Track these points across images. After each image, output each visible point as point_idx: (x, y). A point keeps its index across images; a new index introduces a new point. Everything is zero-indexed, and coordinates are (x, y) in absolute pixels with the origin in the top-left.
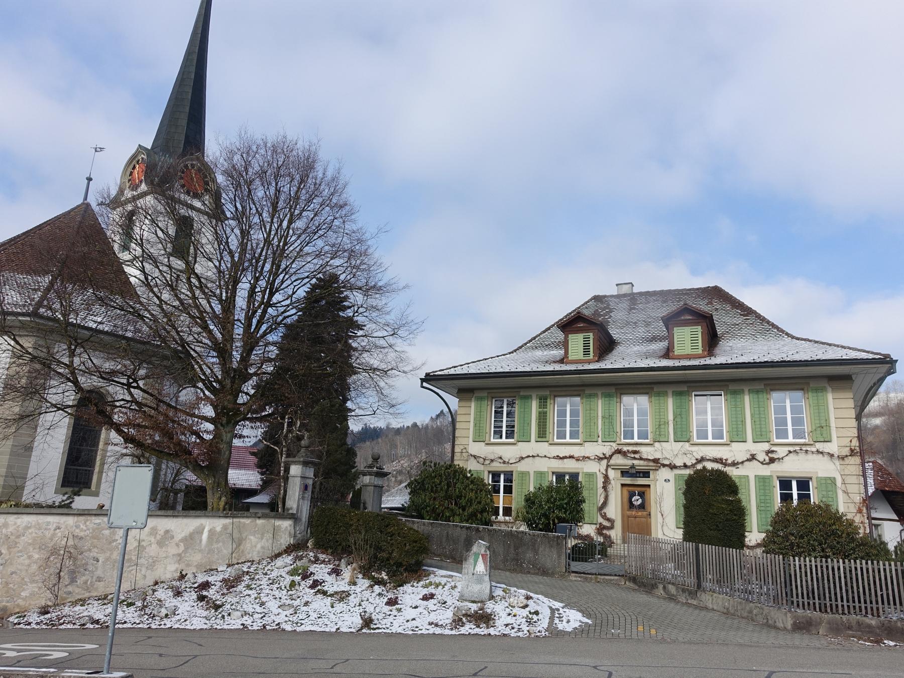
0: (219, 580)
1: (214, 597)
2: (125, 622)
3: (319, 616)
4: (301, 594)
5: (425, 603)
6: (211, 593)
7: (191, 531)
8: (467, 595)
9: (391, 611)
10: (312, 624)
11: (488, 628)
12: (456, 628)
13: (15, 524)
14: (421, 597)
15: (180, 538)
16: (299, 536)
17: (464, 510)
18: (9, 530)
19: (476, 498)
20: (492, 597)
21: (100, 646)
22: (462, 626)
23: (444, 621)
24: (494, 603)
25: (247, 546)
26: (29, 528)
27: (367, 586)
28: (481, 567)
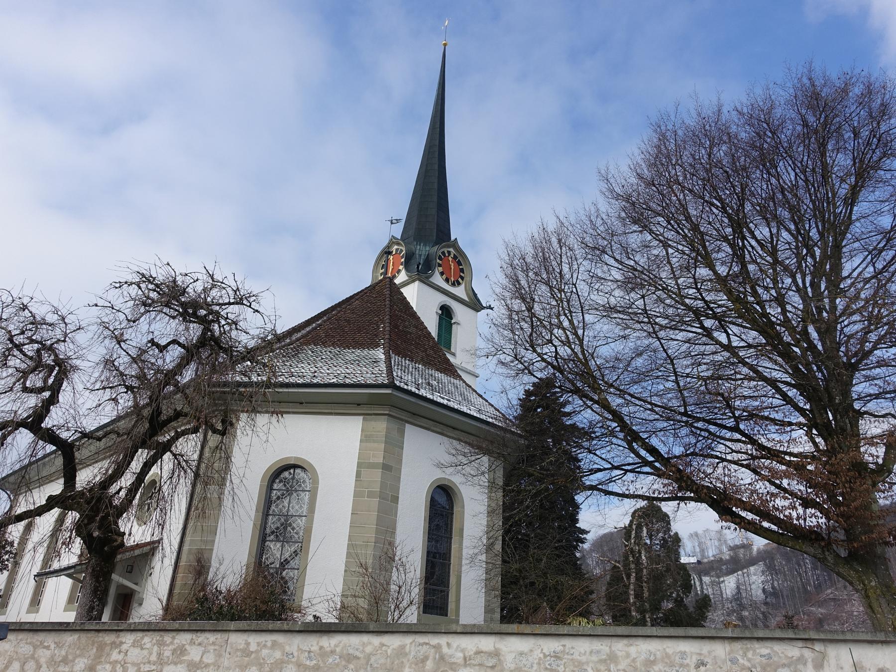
13: (628, 655)
26: (653, 662)
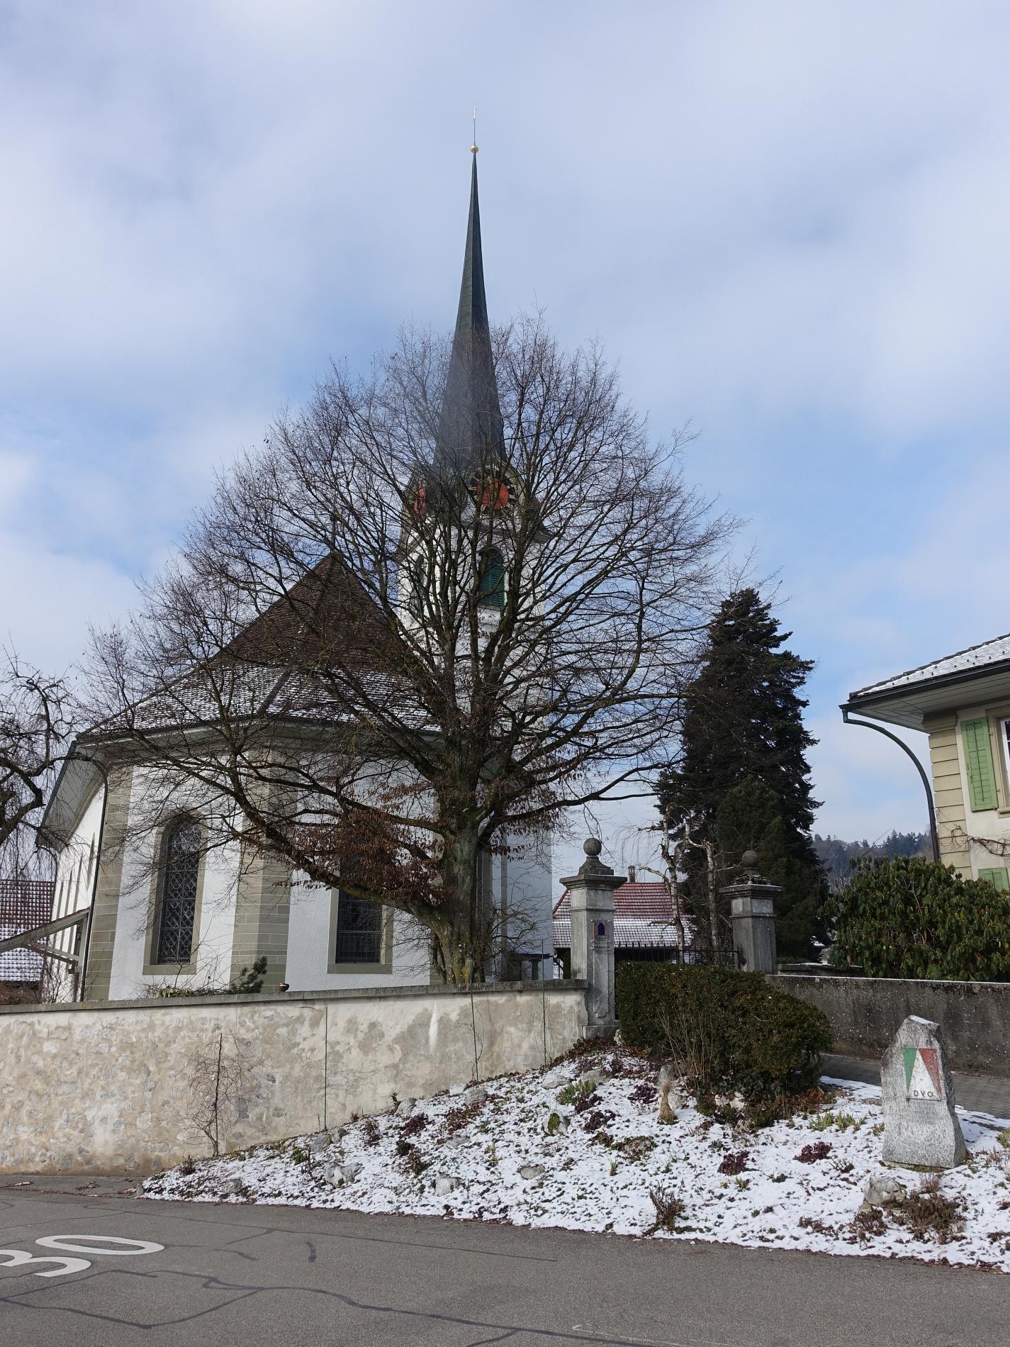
0: (443, 1112)
1: (425, 1146)
2: (280, 1194)
3: (580, 1193)
4: (566, 1143)
5: (805, 1167)
6: (423, 1141)
7: (411, 1022)
8: (901, 1152)
9: (726, 1186)
10: (563, 1213)
11: (944, 1242)
12: (863, 1237)
13: (163, 1023)
14: (799, 1152)
15: (394, 1036)
16: (601, 1022)
17: (944, 950)
18: (156, 1034)
19: (971, 922)
20: (963, 1157)
21: (166, 1246)
22: (879, 1233)
23: (835, 1217)
24: (969, 1172)
25: (505, 1045)
27: (698, 1124)
28: (923, 1082)
